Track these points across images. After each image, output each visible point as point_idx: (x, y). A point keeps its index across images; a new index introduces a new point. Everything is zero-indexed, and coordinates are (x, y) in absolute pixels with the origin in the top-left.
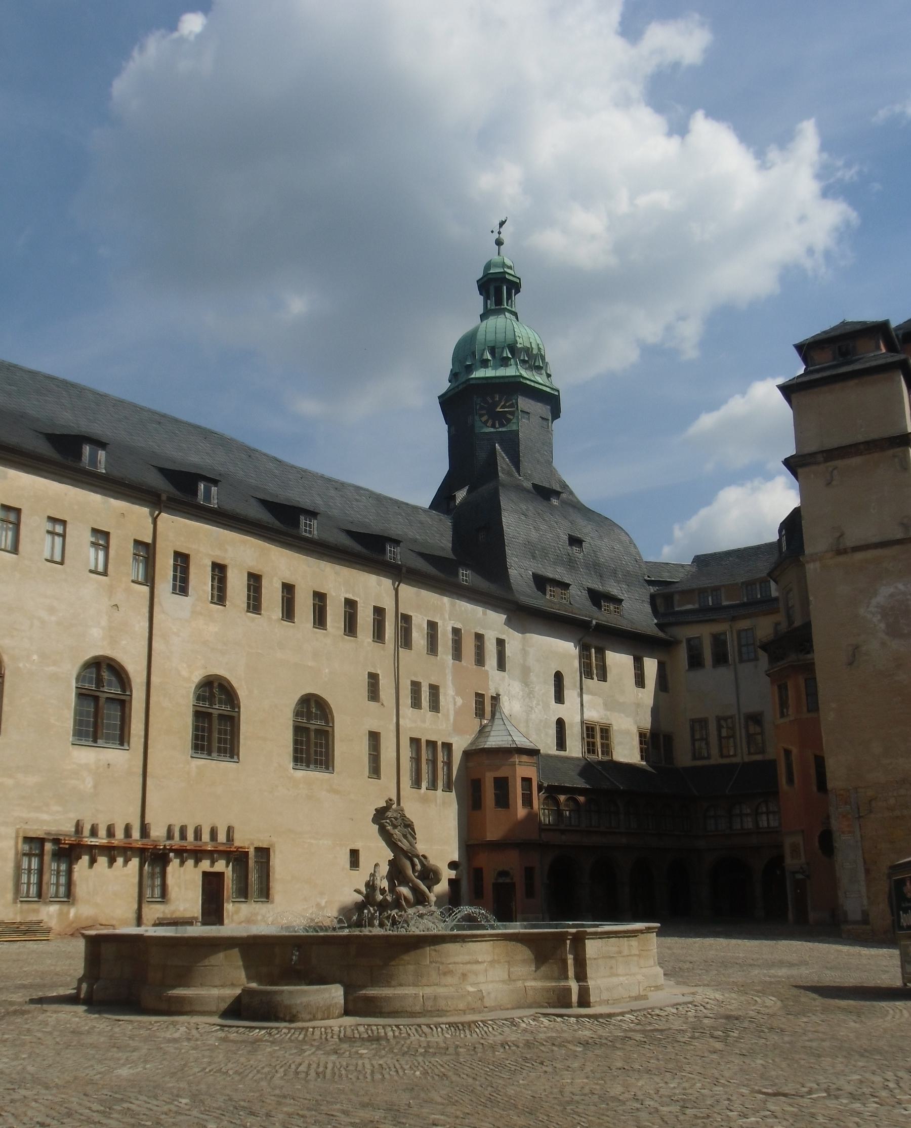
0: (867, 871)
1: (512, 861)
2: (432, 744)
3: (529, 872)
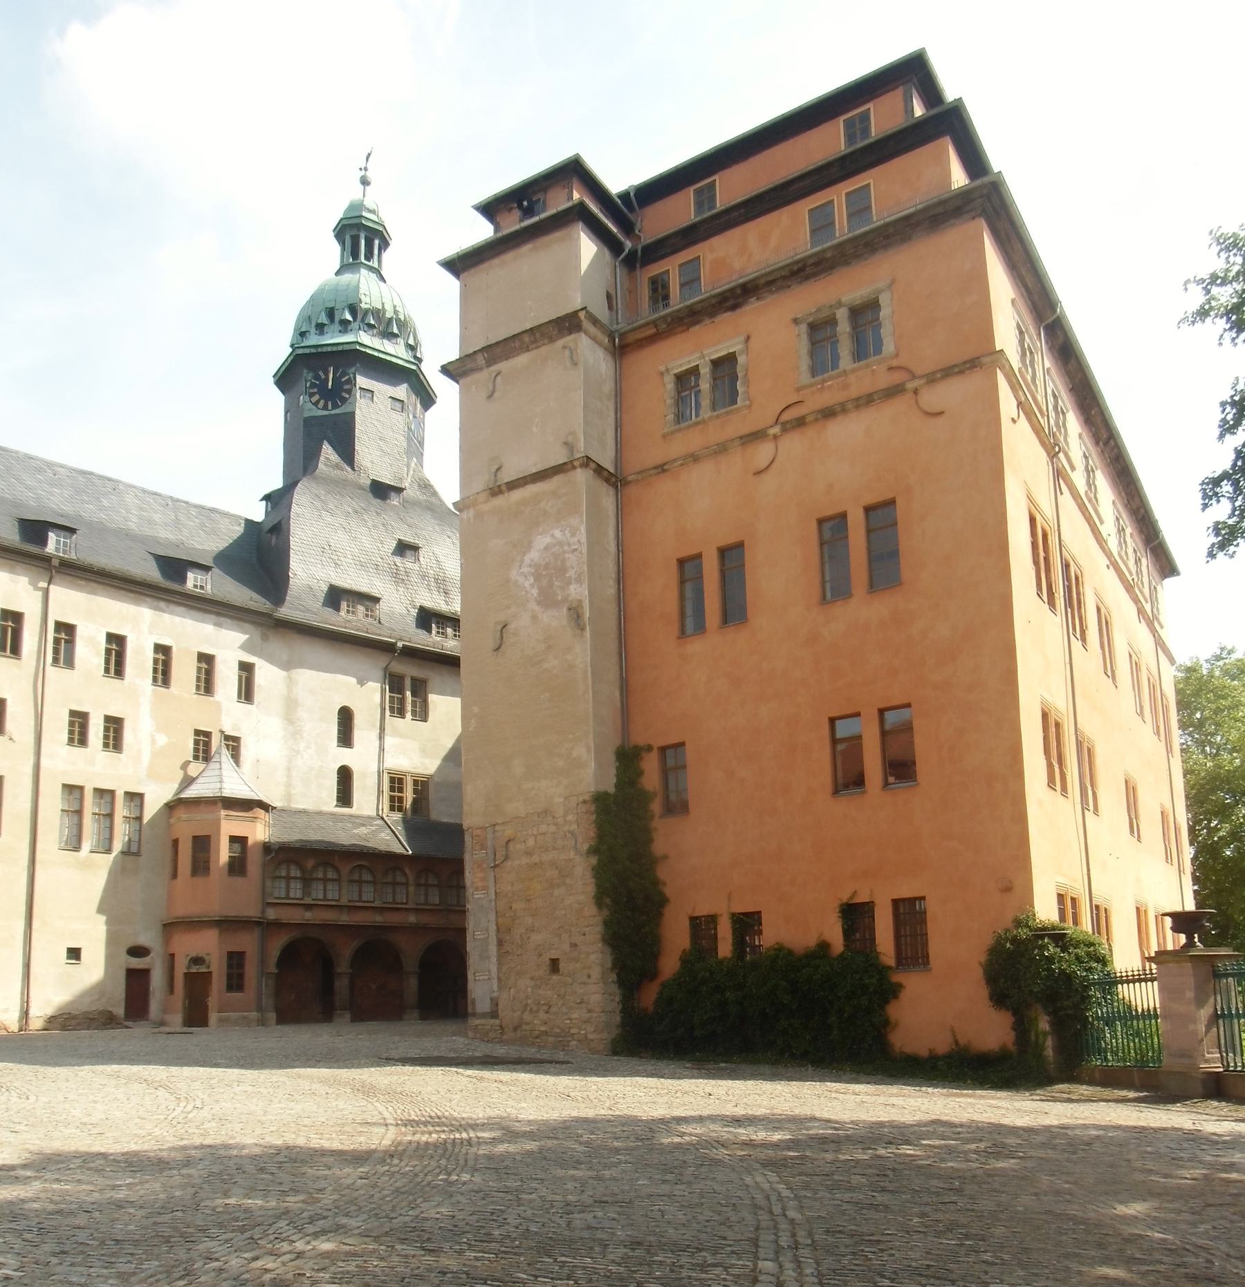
0: (500, 943)
1: (208, 944)
2: (105, 794)
3: (235, 960)
